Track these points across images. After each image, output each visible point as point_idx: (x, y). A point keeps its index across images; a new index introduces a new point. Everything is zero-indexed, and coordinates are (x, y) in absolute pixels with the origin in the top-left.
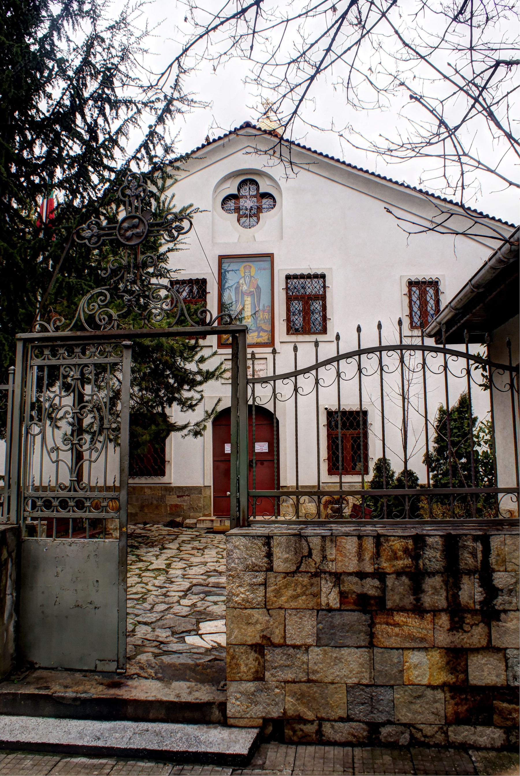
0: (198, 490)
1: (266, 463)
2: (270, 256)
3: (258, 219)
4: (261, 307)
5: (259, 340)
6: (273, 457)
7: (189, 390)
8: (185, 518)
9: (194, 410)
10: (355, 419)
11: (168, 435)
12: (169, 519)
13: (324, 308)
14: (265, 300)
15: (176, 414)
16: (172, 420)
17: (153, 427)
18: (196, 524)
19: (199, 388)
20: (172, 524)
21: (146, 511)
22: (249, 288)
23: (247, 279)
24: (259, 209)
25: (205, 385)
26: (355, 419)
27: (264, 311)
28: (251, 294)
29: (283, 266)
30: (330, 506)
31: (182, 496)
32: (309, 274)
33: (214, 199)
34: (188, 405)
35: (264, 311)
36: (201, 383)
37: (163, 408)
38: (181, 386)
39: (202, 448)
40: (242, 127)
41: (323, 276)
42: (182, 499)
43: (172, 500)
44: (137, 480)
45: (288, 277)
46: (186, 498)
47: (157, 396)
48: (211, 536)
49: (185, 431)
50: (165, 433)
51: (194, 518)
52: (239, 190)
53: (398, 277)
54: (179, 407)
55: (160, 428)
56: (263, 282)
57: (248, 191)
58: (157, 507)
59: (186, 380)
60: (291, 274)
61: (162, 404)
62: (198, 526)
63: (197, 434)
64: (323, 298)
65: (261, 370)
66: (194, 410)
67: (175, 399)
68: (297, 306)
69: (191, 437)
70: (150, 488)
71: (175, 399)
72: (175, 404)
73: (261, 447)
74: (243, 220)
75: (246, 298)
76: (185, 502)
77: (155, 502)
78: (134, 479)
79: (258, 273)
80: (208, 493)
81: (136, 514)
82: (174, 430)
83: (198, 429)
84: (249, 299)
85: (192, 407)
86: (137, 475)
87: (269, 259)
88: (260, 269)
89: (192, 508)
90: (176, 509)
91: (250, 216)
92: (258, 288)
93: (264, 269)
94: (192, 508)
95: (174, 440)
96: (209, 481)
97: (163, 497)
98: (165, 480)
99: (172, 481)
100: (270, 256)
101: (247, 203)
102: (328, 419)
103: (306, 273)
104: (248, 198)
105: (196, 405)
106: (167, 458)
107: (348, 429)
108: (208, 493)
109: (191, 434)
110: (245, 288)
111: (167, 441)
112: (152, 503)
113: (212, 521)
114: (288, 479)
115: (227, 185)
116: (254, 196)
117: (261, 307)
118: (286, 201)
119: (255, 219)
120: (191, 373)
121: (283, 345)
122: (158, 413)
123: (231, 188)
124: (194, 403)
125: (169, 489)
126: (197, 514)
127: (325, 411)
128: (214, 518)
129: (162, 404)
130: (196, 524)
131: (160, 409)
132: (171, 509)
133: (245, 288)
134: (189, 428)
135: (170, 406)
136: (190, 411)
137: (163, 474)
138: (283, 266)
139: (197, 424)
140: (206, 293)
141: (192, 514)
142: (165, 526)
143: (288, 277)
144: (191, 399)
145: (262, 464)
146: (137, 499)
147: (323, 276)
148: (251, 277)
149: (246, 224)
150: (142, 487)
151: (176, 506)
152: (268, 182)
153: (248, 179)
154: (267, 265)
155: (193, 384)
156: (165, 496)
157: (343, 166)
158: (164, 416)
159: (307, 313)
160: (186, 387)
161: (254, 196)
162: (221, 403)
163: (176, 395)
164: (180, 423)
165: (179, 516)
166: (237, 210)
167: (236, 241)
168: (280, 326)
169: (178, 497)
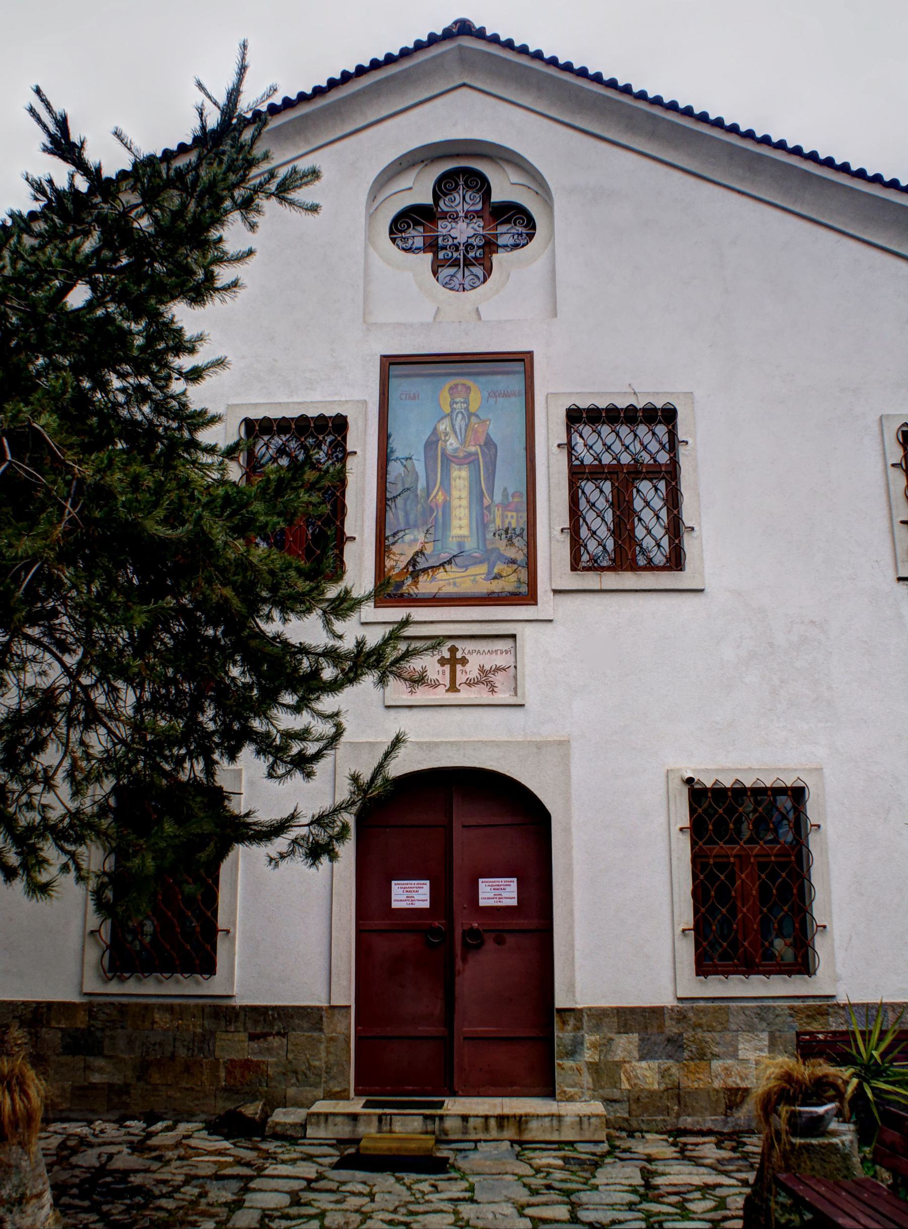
0: (311, 1017)
1: (510, 940)
2: (524, 360)
3: (489, 271)
4: (498, 498)
5: (496, 587)
6: (535, 918)
7: (296, 709)
8: (272, 1104)
9: (309, 775)
10: (730, 811)
11: (223, 852)
12: (222, 1106)
13: (673, 500)
14: (509, 480)
15: (250, 784)
16: (239, 806)
17: (169, 827)
18: (304, 1126)
19: (327, 703)
20: (231, 1126)
21: (156, 1078)
22: (463, 443)
23: (459, 422)
24: (490, 246)
25: (349, 691)
26: (730, 811)
27: (505, 506)
28: (469, 460)
29: (558, 388)
30: (784, 1110)
31: (264, 1036)
32: (631, 409)
33: (371, 217)
34: (292, 758)
35: (505, 506)
36: (334, 686)
37: (210, 767)
38: (269, 698)
39: (325, 893)
40: (448, 34)
41: (669, 416)
42: (263, 1044)
43: (235, 1046)
44: (132, 987)
45: (574, 417)
46: (276, 1042)
47: (193, 725)
48: (355, 1180)
49: (281, 843)
50: (211, 848)
51: (298, 1104)
52: (436, 197)
53: (872, 420)
54: (262, 764)
55: (195, 829)
56: (504, 427)
57: (462, 201)
58: (187, 1069)
59: (292, 675)
60: (584, 404)
61: (206, 753)
62: (310, 1132)
63: (316, 852)
64: (670, 474)
65: (498, 669)
66: (309, 775)
67: (248, 735)
68: (599, 494)
69: (298, 865)
70: (170, 1009)
71: (248, 735)
72: (248, 752)
73: (498, 892)
74: (445, 272)
75: (455, 473)
76: (272, 1054)
77: (182, 1053)
78: (122, 980)
79: (488, 404)
80: (341, 1028)
81: (124, 1089)
82: (241, 839)
83: (323, 838)
84: (464, 473)
85: (303, 764)
86: (133, 970)
87: (519, 367)
88: (494, 394)
89: (291, 1072)
90: (246, 1078)
91: (467, 264)
92: (489, 444)
93: (506, 395)
94: (291, 1072)
95: (244, 865)
96: (345, 993)
97: (207, 1037)
98: (214, 986)
99: (236, 991)
100: (524, 360)
101: (462, 231)
102: (692, 811)
103: (622, 403)
104: (463, 214)
105: (318, 756)
106: (222, 922)
107: (711, 841)
108: (341, 1028)
109: (300, 851)
110: (452, 443)
111: (225, 868)
112: (173, 1057)
113: (354, 1117)
114: (578, 986)
115: (407, 180)
116: (478, 214)
117: (498, 498)
118: (565, 226)
119: (478, 271)
120: (304, 650)
121: (561, 598)
122: (194, 782)
123: (418, 189)
124: (312, 748)
125: (224, 1014)
126: (309, 1092)
127: (685, 790)
128: (356, 1106)
129: (206, 753)
130: (304, 1126)
131: (199, 766)
132: (229, 1073)
133: (452, 443)
134: (293, 833)
135: (232, 758)
136: (298, 775)
137: (208, 967)
138: (558, 388)
139: (319, 821)
140: (346, 454)
141: (291, 1091)
142: (213, 1128)
143: (574, 417)
144: (303, 735)
145: (500, 941)
146: (130, 1042)
147: (669, 416)
148: (470, 415)
149: (456, 282)
150: (146, 1007)
151: (247, 1065)
152: (514, 176)
153: (462, 170)
154: (516, 383)
155: (310, 687)
156: (213, 1033)
157: (716, 133)
158: (218, 796)
159: (624, 517)
160: (289, 698)
161: (478, 214)
162: (402, 752)
163: (257, 724)
164: (265, 815)
165: (254, 1099)
166: (432, 246)
167: (430, 319)
168: (552, 548)
169: (253, 1037)
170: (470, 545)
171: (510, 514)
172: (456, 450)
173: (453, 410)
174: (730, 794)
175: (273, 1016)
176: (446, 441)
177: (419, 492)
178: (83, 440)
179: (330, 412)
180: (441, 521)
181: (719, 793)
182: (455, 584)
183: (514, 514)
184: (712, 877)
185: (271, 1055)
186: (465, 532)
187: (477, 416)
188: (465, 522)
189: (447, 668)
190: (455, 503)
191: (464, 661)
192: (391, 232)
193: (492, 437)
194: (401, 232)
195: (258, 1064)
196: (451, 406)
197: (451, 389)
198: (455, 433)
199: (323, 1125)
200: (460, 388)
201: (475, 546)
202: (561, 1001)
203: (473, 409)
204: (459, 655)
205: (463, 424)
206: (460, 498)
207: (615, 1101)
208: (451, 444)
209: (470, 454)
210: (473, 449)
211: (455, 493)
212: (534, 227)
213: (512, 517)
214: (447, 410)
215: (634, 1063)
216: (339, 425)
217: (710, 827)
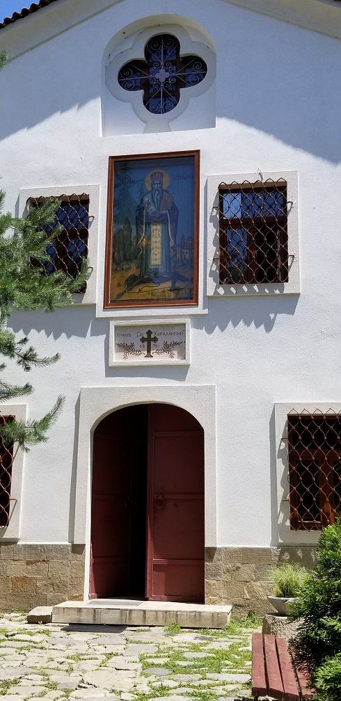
46: (43, 565)
110: (152, 208)
148: (163, 191)
151: (24, 579)
170: (162, 270)
171: (185, 251)
172: (154, 213)
173: (153, 188)
174: (300, 418)
175: (41, 551)
176: (148, 208)
177: (132, 240)
178: (157, 567)
179: (78, 193)
180: (144, 256)
181: (306, 419)
182: (152, 294)
183: (188, 251)
184: (300, 469)
185: (39, 574)
186: (158, 262)
187: (167, 192)
188: (159, 256)
189: (146, 343)
190: (153, 245)
191: (155, 340)
192: (120, 77)
193: (176, 204)
194: (126, 77)
195: (31, 579)
196: (152, 186)
197: (152, 175)
198: (154, 201)
199: (62, 614)
200: (157, 175)
201: (165, 270)
202: (207, 545)
203: (165, 187)
204: (152, 336)
205: (159, 197)
206: (156, 242)
207: (240, 606)
208: (152, 209)
209: (163, 215)
210: (164, 212)
211: (153, 239)
212: (206, 70)
213: (187, 253)
214: (149, 188)
215: (252, 582)
216: (83, 201)
217: (313, 437)
